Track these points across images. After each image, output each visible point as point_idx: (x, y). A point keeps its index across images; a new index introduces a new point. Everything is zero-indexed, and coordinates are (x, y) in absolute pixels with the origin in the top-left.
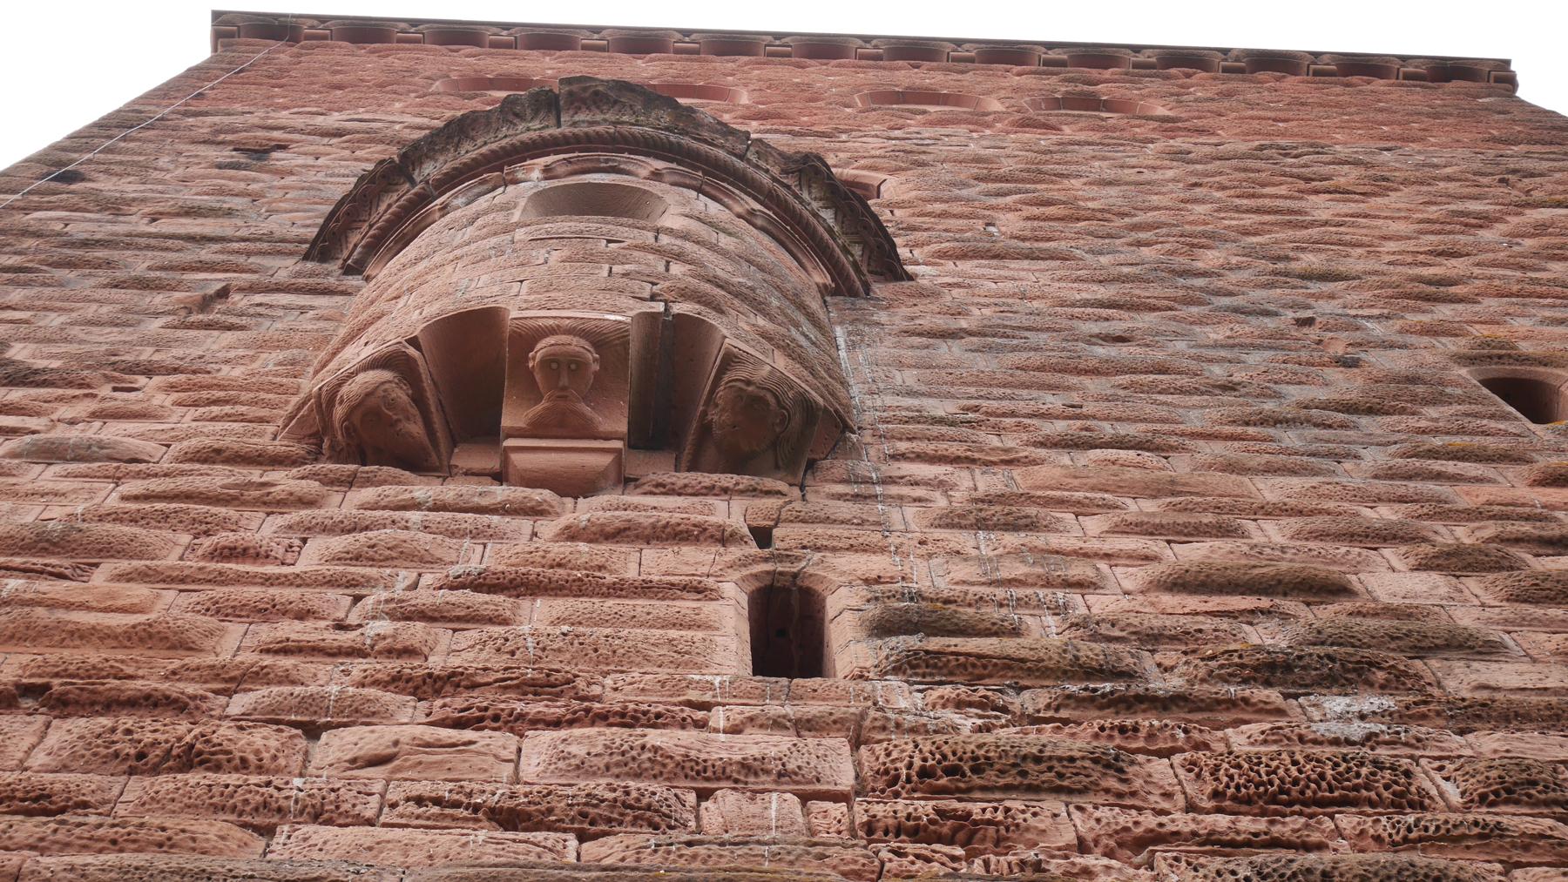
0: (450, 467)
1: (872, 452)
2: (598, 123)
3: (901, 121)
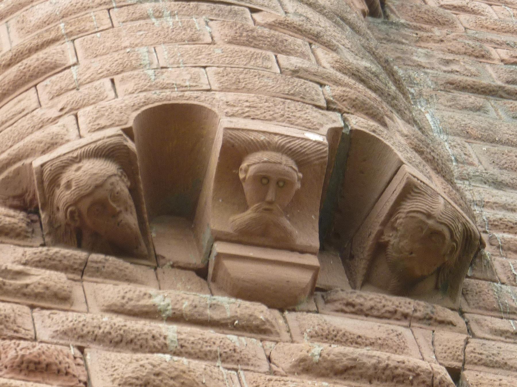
0: (157, 256)
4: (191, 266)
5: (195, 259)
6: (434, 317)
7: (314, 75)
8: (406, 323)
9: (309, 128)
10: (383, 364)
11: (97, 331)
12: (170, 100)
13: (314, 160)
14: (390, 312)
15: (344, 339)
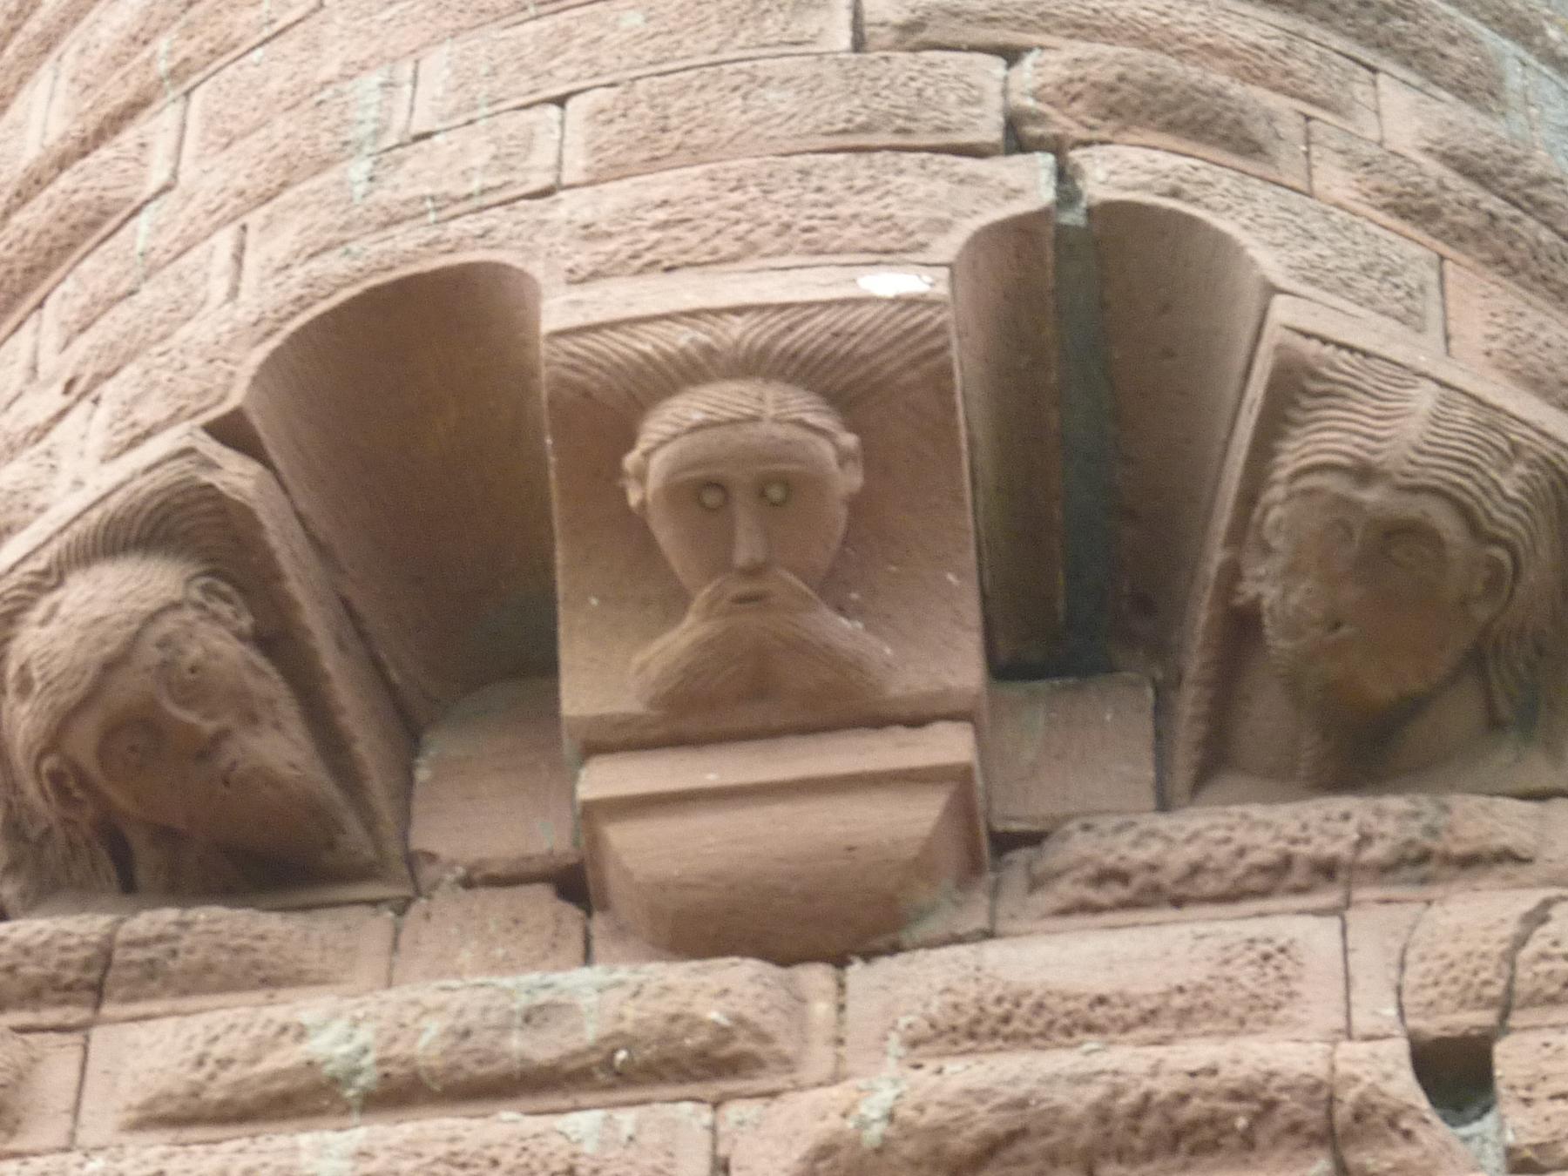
0: (412, 860)
4: (536, 867)
5: (548, 838)
7: (988, 20)
9: (887, 252)
10: (1132, 1097)
12: (390, 268)
13: (901, 370)
14: (1263, 869)
15: (1040, 1023)
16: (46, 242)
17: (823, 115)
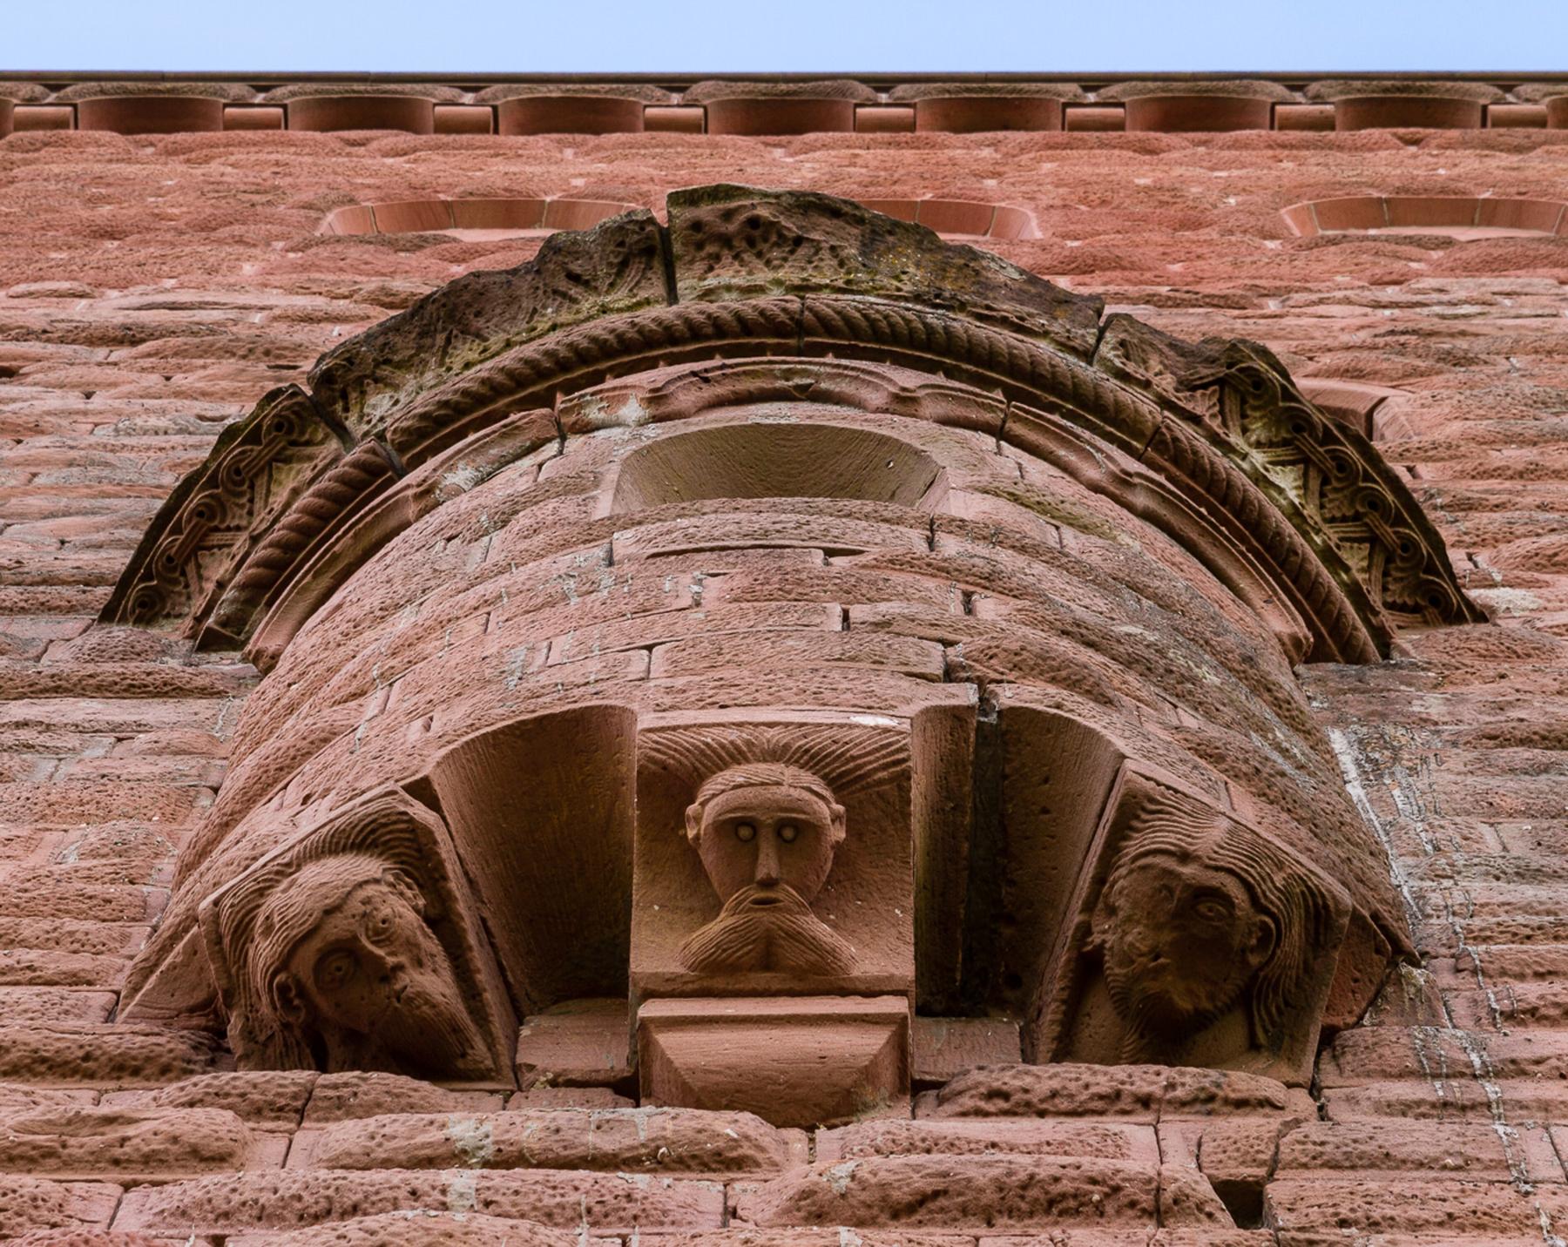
0: (516, 1069)
1: (1460, 1006)
2: (760, 290)
3: (1398, 266)
4: (601, 1077)
5: (612, 1058)
6: (1221, 1093)
8: (1149, 1117)
11: (264, 1198)
13: (876, 770)
14: (1101, 1097)
16: (292, 752)
17: (826, 651)
